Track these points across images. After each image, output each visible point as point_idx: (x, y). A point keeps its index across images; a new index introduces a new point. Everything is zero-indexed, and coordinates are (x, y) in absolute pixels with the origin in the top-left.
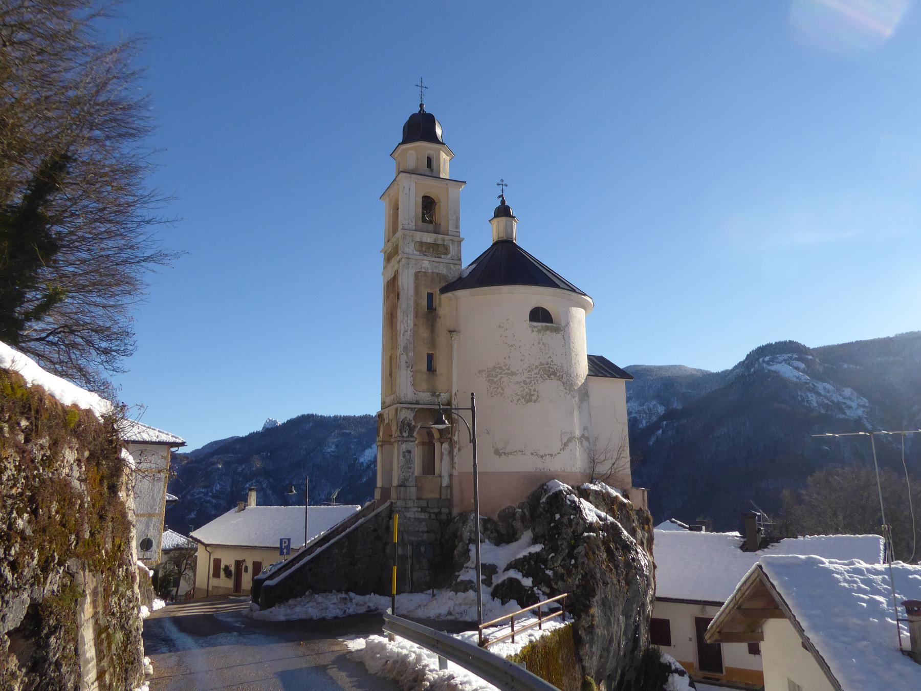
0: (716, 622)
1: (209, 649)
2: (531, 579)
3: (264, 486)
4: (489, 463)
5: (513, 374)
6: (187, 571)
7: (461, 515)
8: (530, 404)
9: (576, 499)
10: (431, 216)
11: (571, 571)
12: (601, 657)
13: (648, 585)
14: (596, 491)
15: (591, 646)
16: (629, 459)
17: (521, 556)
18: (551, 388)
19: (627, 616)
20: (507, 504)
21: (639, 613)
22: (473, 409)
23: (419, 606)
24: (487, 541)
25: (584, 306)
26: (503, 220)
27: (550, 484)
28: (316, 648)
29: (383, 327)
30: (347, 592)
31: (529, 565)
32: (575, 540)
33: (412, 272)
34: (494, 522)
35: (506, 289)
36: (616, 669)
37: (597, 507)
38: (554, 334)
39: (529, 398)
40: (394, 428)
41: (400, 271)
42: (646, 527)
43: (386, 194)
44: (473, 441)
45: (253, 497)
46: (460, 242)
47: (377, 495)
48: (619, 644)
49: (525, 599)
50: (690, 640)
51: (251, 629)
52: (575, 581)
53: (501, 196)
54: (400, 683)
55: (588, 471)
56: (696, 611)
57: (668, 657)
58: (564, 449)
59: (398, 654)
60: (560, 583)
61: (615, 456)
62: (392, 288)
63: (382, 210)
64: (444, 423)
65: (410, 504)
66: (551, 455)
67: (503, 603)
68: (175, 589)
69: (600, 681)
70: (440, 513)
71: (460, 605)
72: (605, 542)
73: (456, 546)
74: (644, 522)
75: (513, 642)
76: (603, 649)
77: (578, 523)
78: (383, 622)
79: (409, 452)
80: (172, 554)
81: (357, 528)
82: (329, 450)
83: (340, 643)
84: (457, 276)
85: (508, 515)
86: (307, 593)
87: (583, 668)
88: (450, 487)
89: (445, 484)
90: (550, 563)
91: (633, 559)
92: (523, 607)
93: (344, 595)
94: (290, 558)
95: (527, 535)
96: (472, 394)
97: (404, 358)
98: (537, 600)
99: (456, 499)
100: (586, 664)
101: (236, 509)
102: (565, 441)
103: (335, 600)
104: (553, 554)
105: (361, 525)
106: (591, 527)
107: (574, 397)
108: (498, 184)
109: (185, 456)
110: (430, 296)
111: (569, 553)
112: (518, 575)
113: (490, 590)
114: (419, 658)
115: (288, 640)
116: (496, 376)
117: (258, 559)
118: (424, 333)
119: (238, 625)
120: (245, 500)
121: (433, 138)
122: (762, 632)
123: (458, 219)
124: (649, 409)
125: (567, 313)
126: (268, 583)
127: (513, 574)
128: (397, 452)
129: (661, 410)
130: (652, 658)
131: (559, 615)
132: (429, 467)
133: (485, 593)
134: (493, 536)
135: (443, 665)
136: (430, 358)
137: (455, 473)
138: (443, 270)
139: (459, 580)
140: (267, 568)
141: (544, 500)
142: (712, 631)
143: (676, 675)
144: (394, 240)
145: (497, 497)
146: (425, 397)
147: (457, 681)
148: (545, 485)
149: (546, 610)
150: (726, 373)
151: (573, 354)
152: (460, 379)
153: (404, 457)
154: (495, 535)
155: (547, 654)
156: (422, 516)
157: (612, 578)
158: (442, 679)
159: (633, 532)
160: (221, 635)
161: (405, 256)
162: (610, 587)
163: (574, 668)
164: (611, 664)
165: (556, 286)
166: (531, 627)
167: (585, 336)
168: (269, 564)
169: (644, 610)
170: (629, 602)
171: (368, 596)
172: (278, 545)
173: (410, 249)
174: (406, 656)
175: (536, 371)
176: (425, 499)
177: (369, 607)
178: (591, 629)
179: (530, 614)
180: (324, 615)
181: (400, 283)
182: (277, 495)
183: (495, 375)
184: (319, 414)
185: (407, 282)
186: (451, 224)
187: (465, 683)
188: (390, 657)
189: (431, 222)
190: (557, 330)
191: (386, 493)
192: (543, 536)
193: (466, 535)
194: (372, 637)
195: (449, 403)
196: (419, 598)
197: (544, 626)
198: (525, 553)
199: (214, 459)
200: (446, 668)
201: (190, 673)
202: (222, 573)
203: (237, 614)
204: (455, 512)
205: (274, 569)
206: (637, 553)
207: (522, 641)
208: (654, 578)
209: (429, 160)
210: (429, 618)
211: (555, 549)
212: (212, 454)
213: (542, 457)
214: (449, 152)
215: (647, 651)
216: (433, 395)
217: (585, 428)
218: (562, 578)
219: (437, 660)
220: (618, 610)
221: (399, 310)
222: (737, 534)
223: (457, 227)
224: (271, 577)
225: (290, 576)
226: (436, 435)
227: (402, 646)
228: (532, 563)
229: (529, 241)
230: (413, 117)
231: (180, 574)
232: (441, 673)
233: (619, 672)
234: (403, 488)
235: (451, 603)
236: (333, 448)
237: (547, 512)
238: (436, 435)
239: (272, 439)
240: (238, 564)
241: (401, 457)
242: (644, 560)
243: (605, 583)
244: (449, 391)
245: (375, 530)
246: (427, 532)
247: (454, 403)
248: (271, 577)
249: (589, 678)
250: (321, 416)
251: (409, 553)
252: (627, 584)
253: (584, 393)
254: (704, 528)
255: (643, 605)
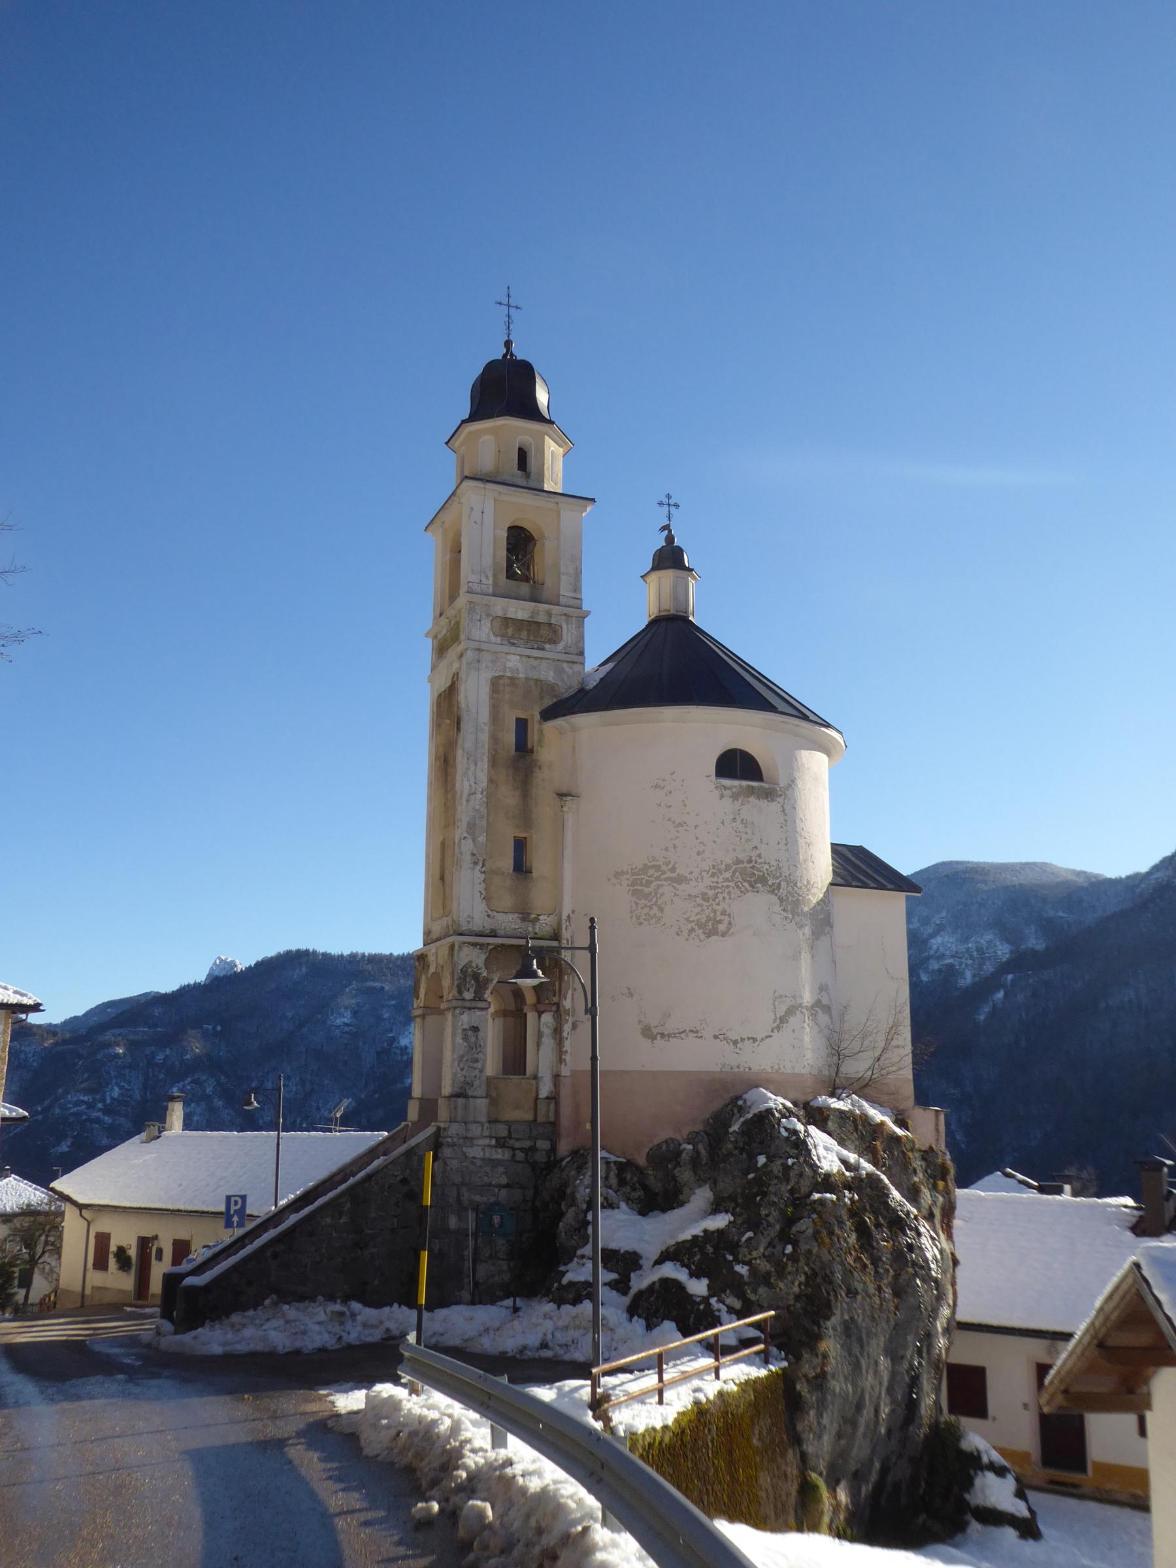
0: (1058, 1372)
1: (66, 1405)
2: (705, 1282)
3: (209, 1090)
4: (625, 1051)
5: (681, 880)
6: (46, 1257)
7: (575, 1153)
8: (715, 937)
9: (800, 1127)
10: (527, 565)
11: (785, 1267)
12: (839, 1436)
13: (940, 1298)
14: (840, 1112)
15: (820, 1415)
16: (909, 1048)
17: (687, 1235)
18: (756, 907)
19: (895, 1357)
20: (666, 1133)
21: (919, 1351)
22: (592, 948)
23: (487, 1330)
24: (623, 1205)
25: (826, 748)
26: (669, 575)
27: (750, 1096)
28: (273, 1407)
29: (430, 785)
30: (346, 1300)
31: (701, 1254)
32: (795, 1206)
33: (486, 676)
34: (639, 1170)
35: (670, 713)
36: (871, 1461)
37: (841, 1143)
38: (763, 803)
39: (712, 928)
40: (446, 982)
41: (463, 675)
42: (941, 1184)
43: (438, 522)
44: (591, 1011)
45: (177, 1113)
46: (582, 618)
47: (413, 1112)
48: (877, 1411)
49: (691, 1318)
50: (1026, 1406)
51: (151, 1366)
52: (792, 1286)
53: (666, 528)
54: (419, 1474)
55: (826, 1073)
56: (1036, 1349)
57: (976, 1438)
58: (778, 1028)
59: (420, 1419)
60: (762, 1290)
61: (882, 1044)
62: (447, 708)
63: (427, 555)
64: (534, 975)
65: (475, 1130)
66: (755, 1040)
67: (650, 1327)
68: (23, 1292)
69: (838, 1482)
70: (533, 1149)
71: (566, 1328)
72: (855, 1213)
73: (562, 1215)
74: (937, 1174)
75: (661, 1402)
76: (845, 1420)
77: (801, 1175)
78: (400, 1359)
79: (475, 1029)
80: (17, 1222)
81: (369, 1177)
82: (338, 1022)
83: (321, 1398)
84: (576, 686)
85: (665, 1157)
86: (267, 1302)
87: (803, 1456)
88: (554, 1098)
89: (544, 1092)
90: (744, 1250)
91: (910, 1247)
92: (685, 1336)
93: (338, 1307)
94: (239, 1232)
95: (702, 1196)
96: (592, 920)
97: (467, 847)
98: (716, 1322)
99: (565, 1121)
100: (810, 1449)
101: (143, 1136)
102: (781, 1013)
103: (322, 1317)
104: (750, 1234)
105: (377, 1172)
106: (827, 1183)
107: (801, 927)
108: (661, 504)
109: (50, 1030)
110: (522, 725)
111: (782, 1230)
112: (682, 1275)
113: (626, 1300)
114: (456, 1428)
115: (219, 1392)
116: (648, 883)
117: (183, 1235)
118: (509, 797)
119: (128, 1361)
120: (160, 1117)
121: (530, 411)
122: (1149, 1394)
123: (578, 573)
124: (979, 950)
125: (791, 763)
126: (190, 1281)
127: (670, 1270)
128: (452, 1027)
129: (1003, 951)
130: (944, 1440)
131: (757, 1353)
132: (515, 1060)
133: (612, 1308)
134: (635, 1195)
135: (498, 1441)
136: (520, 846)
137: (565, 1071)
138: (548, 675)
139: (565, 1281)
140: (198, 1254)
141: (735, 1127)
142: (1051, 1390)
143: (990, 1476)
144: (451, 612)
145: (655, 1122)
146: (508, 922)
147: (518, 1469)
148: (739, 1098)
149: (733, 1342)
150: (1134, 881)
151: (801, 841)
152: (579, 886)
153: (465, 1038)
154: (640, 1193)
155: (728, 1427)
156: (500, 1154)
157: (865, 1282)
158: (491, 1466)
159: (913, 1194)
160: (93, 1379)
161: (473, 645)
162: (864, 1298)
163: (783, 1455)
164: (860, 1450)
165: (769, 707)
166: (699, 1374)
167: (825, 806)
168: (206, 1240)
169: (930, 1347)
170: (898, 1331)
171: (386, 1309)
172: (222, 1208)
173: (483, 631)
174: (434, 1423)
175: (728, 875)
176: (506, 1122)
177: (388, 1330)
178: (820, 1381)
179: (698, 1349)
180: (298, 1344)
181: (461, 698)
182: (228, 1106)
183: (645, 882)
184: (321, 949)
185: (475, 696)
186: (565, 581)
187: (530, 1474)
188: (405, 1425)
189: (526, 579)
190: (770, 795)
191: (429, 1108)
192: (732, 1198)
193: (583, 1193)
194: (378, 1387)
195: (556, 937)
196: (485, 1315)
197: (723, 1373)
198: (697, 1230)
199: (108, 1036)
200: (505, 1446)
201: (23, 1449)
202: (112, 1262)
203: (132, 1341)
204: (564, 1147)
205: (208, 1254)
206: (919, 1234)
207: (679, 1401)
208: (953, 1284)
209: (523, 455)
210: (504, 1353)
211: (755, 1224)
212: (102, 1028)
213: (735, 1043)
214: (563, 438)
215: (935, 1427)
216: (524, 920)
217: (823, 988)
218: (766, 1280)
219: (489, 1431)
220: (876, 1346)
221: (459, 753)
222: (1129, 1201)
223: (577, 588)
224: (198, 1270)
225: (235, 1268)
226: (530, 998)
227: (434, 1406)
228: (710, 1249)
229: (720, 618)
230: (491, 367)
231: (33, 1261)
232: (491, 1455)
233: (877, 1465)
234: (460, 1101)
235: (548, 1325)
236: (347, 1018)
237: (742, 1150)
238: (530, 998)
239: (228, 998)
240: (144, 1243)
241: (459, 1040)
242: (930, 1247)
243: (852, 1293)
244: (556, 911)
245: (404, 1181)
246: (507, 1186)
247: (566, 934)
248: (198, 1270)
249: (814, 1475)
250: (325, 955)
251: (471, 1226)
252: (897, 1293)
253: (823, 920)
254: (1067, 1188)
255: (929, 1337)
